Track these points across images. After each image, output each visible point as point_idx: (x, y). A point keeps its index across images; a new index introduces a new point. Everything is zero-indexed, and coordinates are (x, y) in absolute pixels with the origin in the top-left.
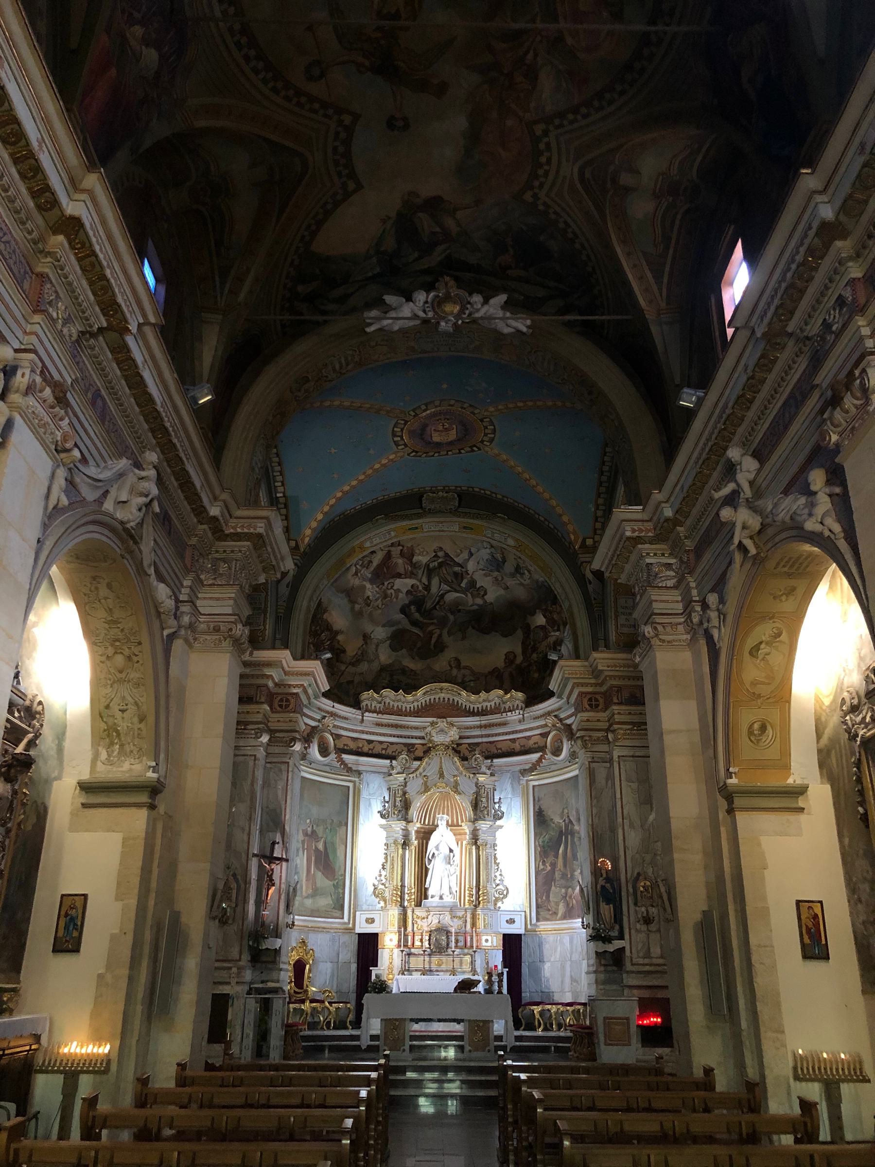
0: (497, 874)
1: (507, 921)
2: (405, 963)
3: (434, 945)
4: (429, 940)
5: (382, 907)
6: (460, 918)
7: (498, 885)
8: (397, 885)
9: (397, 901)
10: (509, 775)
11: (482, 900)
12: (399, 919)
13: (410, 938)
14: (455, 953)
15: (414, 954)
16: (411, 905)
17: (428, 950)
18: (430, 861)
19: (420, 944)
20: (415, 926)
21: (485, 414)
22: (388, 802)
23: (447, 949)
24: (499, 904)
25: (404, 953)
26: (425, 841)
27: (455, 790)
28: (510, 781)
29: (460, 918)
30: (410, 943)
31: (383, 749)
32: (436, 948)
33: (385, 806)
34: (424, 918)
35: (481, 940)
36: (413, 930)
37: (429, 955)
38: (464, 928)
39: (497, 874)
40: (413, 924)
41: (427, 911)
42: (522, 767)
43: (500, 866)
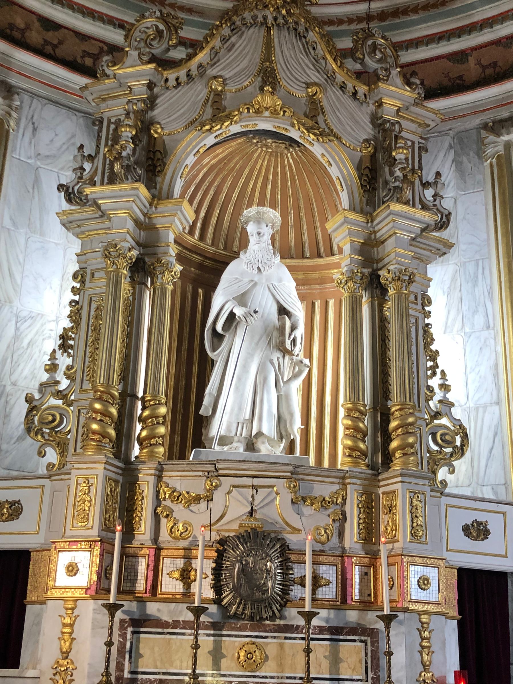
0: (435, 382)
1: (467, 530)
2: (121, 652)
3: (236, 590)
4: (217, 572)
5: (50, 466)
6: (324, 504)
7: (437, 415)
8: (108, 385)
9: (104, 435)
10: (447, 141)
11: (401, 448)
12: (107, 498)
13: (142, 566)
14: (315, 622)
15: (159, 623)
16: (152, 455)
17: (213, 608)
18: (217, 337)
19: (179, 587)
20: (165, 524)
21: (254, 5)
22: (91, 158)
23: (283, 606)
24: (442, 473)
25: (119, 615)
26: (201, 292)
27: (310, 123)
28: (452, 155)
29: (324, 504)
30: (141, 585)
31: (86, 54)
32: (244, 600)
33: (82, 169)
34: (197, 499)
35: (404, 578)
36: (155, 539)
37: (214, 626)
38: (335, 540)
39: (435, 382)
40: (156, 517)
41: (208, 475)
42: (488, 117)
43: (439, 360)
